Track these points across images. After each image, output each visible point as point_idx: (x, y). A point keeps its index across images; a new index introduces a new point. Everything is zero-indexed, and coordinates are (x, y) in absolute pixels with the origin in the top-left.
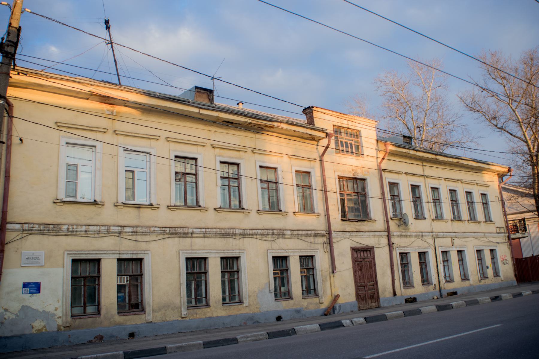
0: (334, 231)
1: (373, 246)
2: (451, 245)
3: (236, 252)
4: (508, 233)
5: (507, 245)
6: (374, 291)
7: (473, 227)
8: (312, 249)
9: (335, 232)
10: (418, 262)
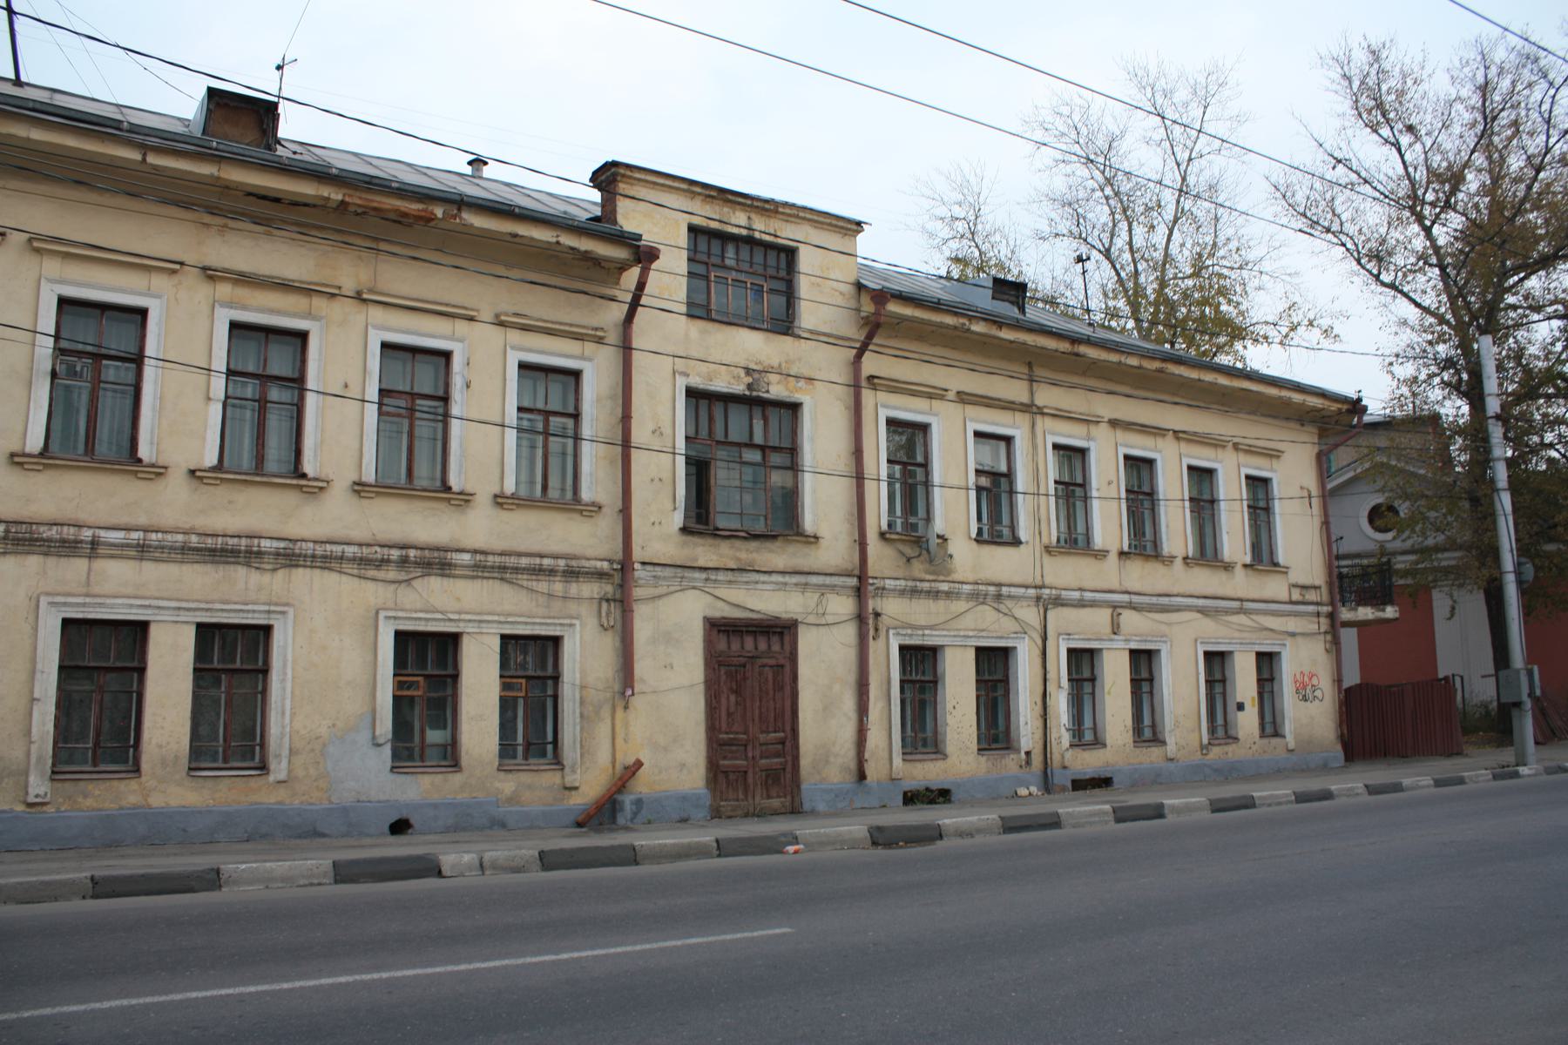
0: (643, 563)
1: (795, 617)
2: (1108, 629)
3: (254, 611)
4: (1332, 603)
5: (1325, 642)
6: (783, 760)
7: (1204, 581)
8: (552, 614)
9: (649, 568)
10: (192, 666)
